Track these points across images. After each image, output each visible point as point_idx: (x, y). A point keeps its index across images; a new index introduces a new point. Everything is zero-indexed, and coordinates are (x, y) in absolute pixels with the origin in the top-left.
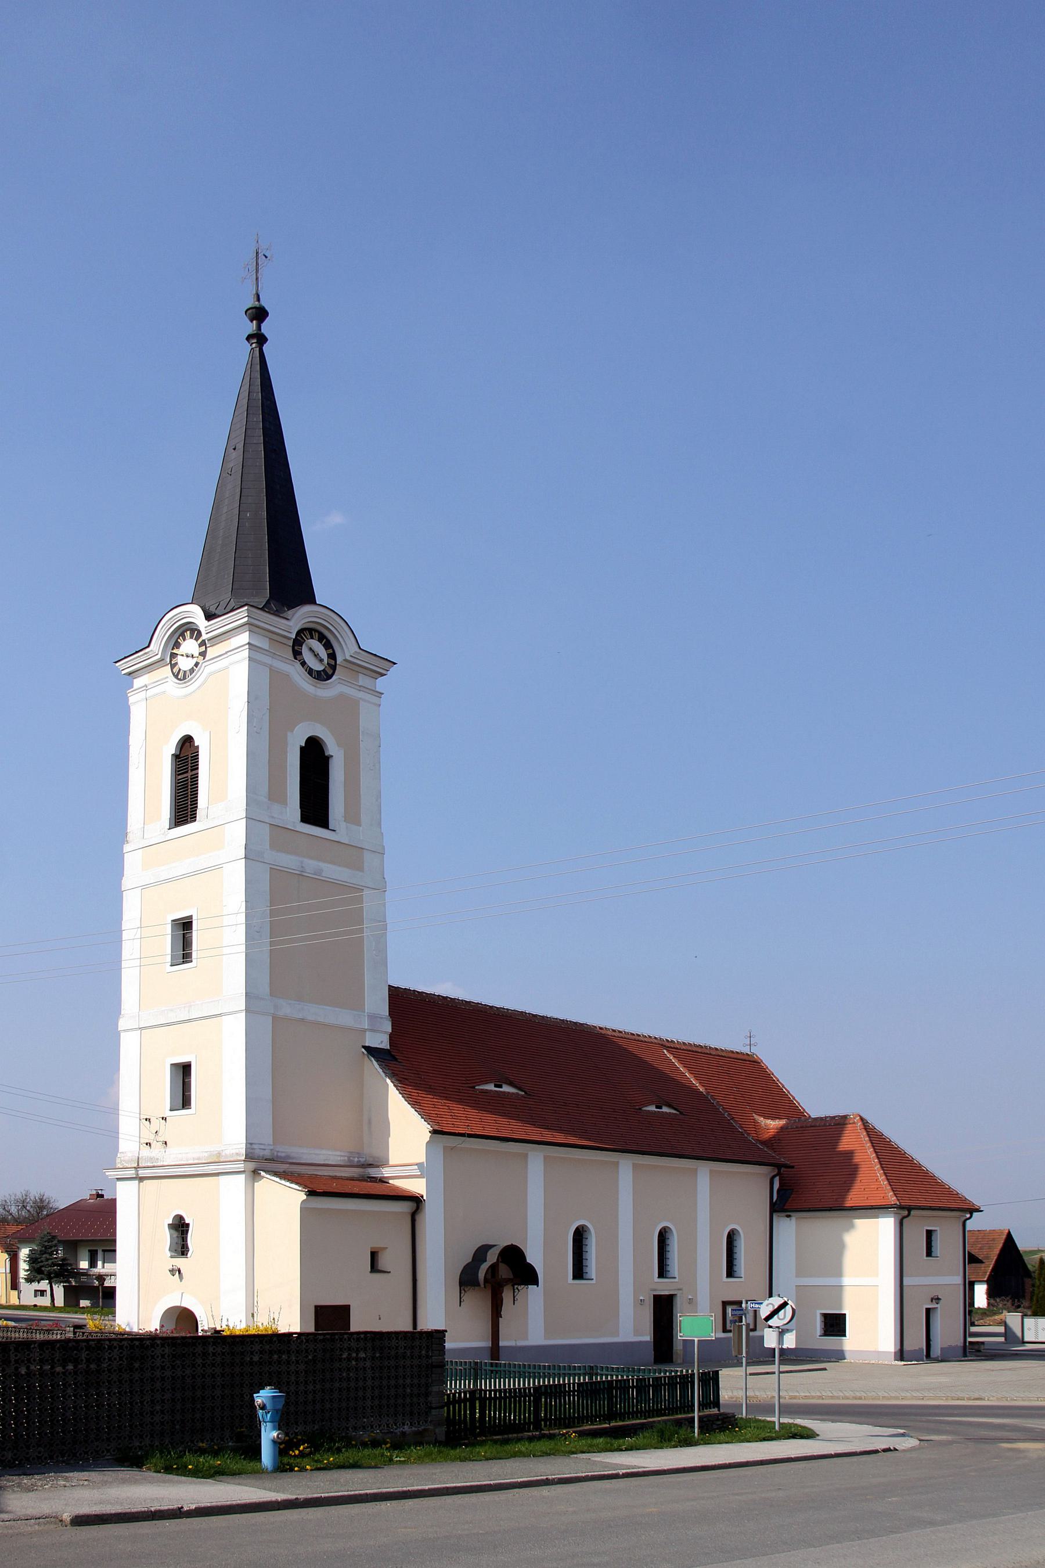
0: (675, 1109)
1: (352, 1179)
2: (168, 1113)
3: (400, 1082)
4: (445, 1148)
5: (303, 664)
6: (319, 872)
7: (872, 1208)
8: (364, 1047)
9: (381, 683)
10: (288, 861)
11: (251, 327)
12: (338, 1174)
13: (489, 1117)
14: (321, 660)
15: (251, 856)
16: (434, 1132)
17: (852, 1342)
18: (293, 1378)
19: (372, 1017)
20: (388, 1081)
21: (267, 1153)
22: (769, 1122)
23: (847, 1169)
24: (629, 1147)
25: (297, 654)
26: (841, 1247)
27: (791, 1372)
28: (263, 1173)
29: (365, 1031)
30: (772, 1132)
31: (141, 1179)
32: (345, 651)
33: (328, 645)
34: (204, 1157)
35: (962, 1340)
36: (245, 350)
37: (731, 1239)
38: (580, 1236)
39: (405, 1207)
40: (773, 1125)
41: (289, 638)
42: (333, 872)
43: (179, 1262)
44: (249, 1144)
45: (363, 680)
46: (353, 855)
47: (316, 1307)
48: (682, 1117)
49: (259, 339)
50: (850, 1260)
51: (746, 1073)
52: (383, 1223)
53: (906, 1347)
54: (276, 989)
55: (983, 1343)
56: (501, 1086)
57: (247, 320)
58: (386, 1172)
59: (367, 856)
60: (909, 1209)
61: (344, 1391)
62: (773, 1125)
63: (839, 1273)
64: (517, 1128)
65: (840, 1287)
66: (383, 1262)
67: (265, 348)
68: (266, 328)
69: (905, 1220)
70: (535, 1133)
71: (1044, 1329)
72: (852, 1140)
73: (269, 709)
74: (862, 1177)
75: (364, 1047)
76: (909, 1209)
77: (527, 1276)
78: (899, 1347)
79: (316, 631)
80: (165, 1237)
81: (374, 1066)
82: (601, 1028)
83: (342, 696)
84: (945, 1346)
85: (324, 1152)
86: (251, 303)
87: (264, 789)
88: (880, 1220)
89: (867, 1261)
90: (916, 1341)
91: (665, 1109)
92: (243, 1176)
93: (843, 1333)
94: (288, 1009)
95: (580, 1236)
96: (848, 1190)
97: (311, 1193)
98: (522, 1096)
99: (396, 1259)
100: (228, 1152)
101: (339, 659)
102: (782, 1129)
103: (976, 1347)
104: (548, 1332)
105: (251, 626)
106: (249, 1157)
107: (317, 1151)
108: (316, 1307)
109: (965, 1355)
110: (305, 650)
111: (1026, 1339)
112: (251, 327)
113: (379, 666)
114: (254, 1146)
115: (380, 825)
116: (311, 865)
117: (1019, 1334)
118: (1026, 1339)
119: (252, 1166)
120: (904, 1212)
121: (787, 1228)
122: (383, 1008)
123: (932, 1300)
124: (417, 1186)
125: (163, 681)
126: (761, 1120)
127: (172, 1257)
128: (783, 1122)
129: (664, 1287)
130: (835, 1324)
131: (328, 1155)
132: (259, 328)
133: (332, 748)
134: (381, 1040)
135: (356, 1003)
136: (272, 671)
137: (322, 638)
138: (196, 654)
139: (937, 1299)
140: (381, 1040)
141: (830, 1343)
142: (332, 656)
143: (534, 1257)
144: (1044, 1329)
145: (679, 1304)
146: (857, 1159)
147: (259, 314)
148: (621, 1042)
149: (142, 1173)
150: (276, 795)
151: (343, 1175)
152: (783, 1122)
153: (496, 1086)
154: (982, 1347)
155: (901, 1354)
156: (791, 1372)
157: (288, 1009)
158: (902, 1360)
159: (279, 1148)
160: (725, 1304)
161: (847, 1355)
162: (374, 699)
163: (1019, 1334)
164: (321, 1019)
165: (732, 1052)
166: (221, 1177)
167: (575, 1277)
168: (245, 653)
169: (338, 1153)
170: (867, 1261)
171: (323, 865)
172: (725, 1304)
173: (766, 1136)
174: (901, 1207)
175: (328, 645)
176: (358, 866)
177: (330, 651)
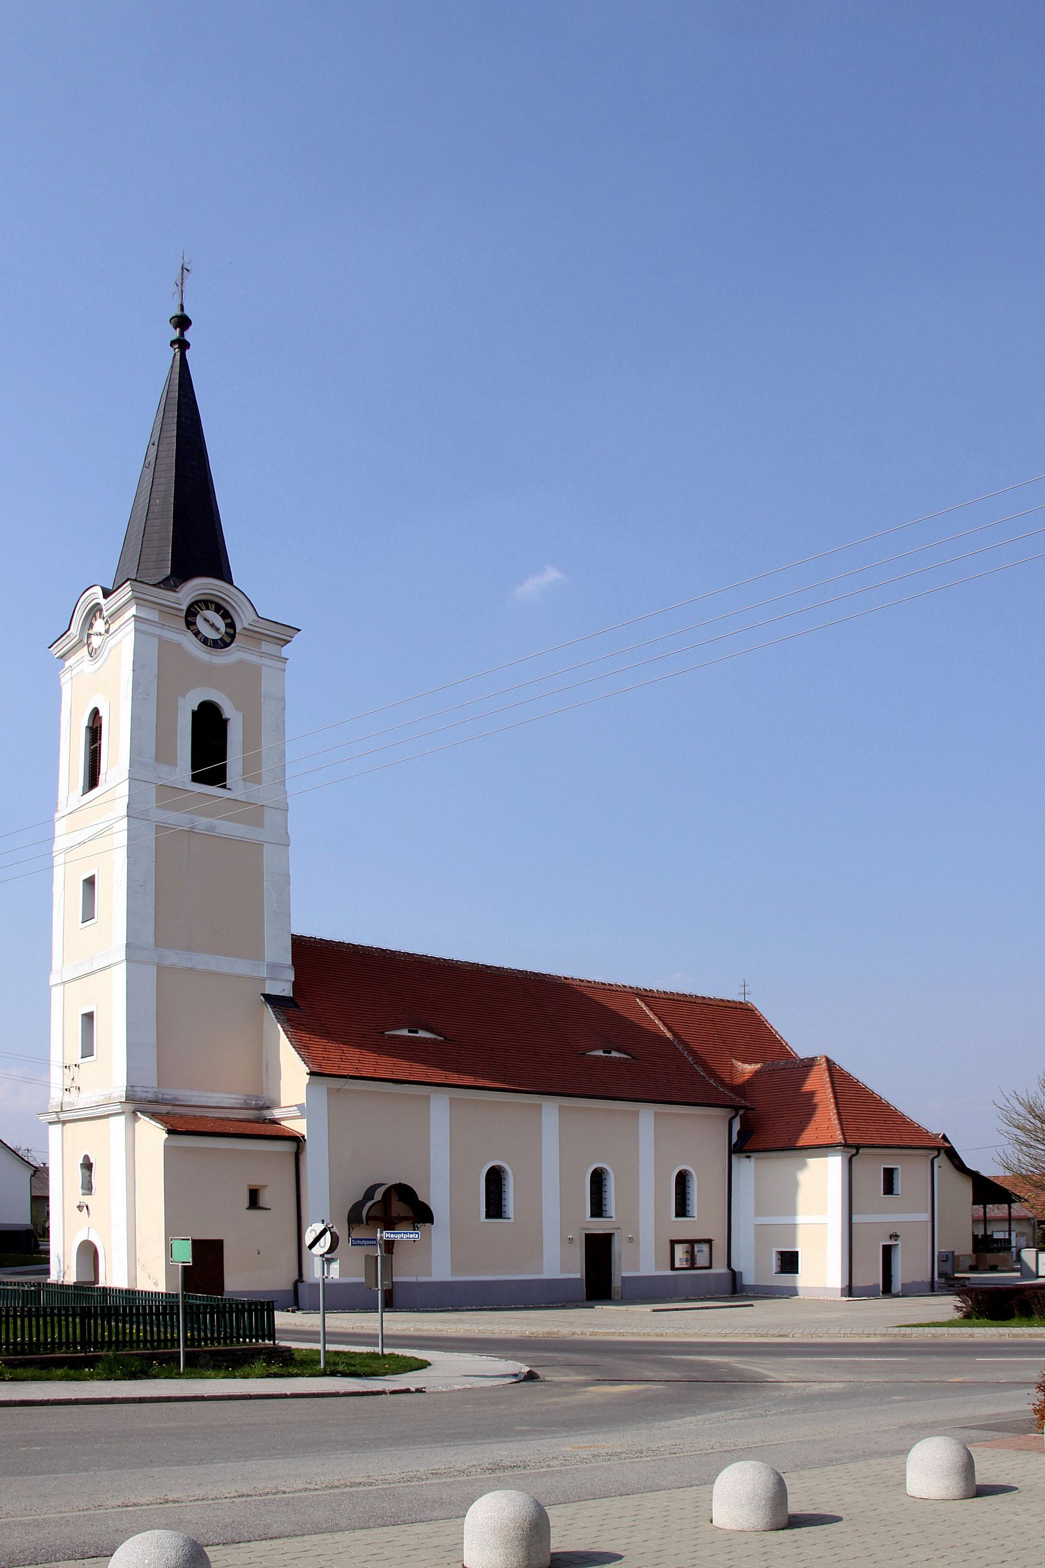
0: (626, 1054)
1: (249, 1121)
2: (80, 1061)
3: (293, 1027)
4: (329, 1090)
5: (197, 633)
6: (213, 828)
7: (820, 1147)
8: (263, 995)
9: (286, 651)
10: (179, 819)
11: (176, 334)
12: (230, 1116)
13: (389, 1061)
14: (218, 630)
15: (133, 814)
16: (311, 1074)
17: (805, 1278)
18: (56, 1311)
19: (272, 966)
20: (279, 1026)
21: (150, 1096)
22: (746, 1066)
23: (807, 1107)
24: (550, 1090)
25: (190, 624)
26: (795, 1185)
27: (707, 1308)
28: (139, 1114)
29: (264, 979)
30: (747, 1077)
31: (64, 1122)
32: (244, 620)
33: (226, 615)
34: (101, 1100)
35: (930, 1276)
36: (170, 353)
37: (682, 1179)
38: (598, 1179)
39: (289, 1147)
40: (748, 1069)
41: (181, 610)
42: (226, 828)
43: (87, 1200)
44: (130, 1087)
45: (266, 647)
46: (253, 813)
47: (222, 1241)
48: (633, 1061)
49: (182, 345)
50: (804, 1197)
51: (740, 1023)
52: (264, 1164)
53: (855, 1283)
54: (161, 940)
55: (968, 1278)
56: (416, 1032)
57: (171, 327)
58: (277, 1114)
59: (268, 813)
60: (858, 1147)
61: (207, 1324)
62: (748, 1069)
63: (793, 1211)
64: (419, 1071)
65: (794, 1226)
66: (264, 1199)
67: (188, 353)
68: (188, 335)
69: (942, 1161)
70: (438, 1075)
71: (1044, 1264)
72: (818, 1083)
73: (156, 678)
74: (819, 1117)
75: (263, 995)
76: (858, 1147)
77: (422, 1215)
78: (847, 1283)
79: (212, 602)
80: (78, 1173)
81: (269, 1011)
82: (566, 978)
83: (241, 662)
84: (909, 1281)
85: (216, 1095)
86: (177, 312)
87: (150, 749)
88: (829, 1158)
89: (817, 1196)
90: (871, 1274)
91: (614, 1054)
92: (123, 1118)
93: (795, 1271)
94: (174, 958)
95: (598, 1179)
96: (802, 1130)
97: (170, 1132)
98: (440, 1041)
99: (277, 1195)
100: (114, 1095)
101: (238, 628)
102: (757, 1073)
103: (961, 1282)
104: (455, 1269)
105: (137, 599)
106: (130, 1098)
107: (209, 1094)
108: (222, 1241)
109: (932, 1289)
110: (199, 621)
111: (1040, 1274)
112: (176, 334)
113: (282, 634)
114: (136, 1089)
115: (283, 783)
116: (202, 822)
117: (1034, 1269)
118: (1040, 1274)
119: (130, 1107)
120: (852, 1149)
121: (746, 1169)
122: (286, 957)
123: (891, 1237)
124: (299, 1127)
125: (80, 662)
126: (739, 1065)
127: (83, 1194)
128: (759, 1066)
129: (599, 1226)
130: (789, 1262)
131: (220, 1096)
132: (182, 334)
133: (228, 711)
134: (283, 988)
135: (255, 952)
136: (162, 642)
137: (219, 609)
138: (103, 632)
139: (894, 1236)
140: (283, 988)
141: (785, 1279)
142: (231, 625)
143: (437, 1196)
144: (1044, 1264)
145: (618, 1247)
146: (817, 1099)
147: (182, 322)
148: (586, 992)
149: (63, 1116)
150: (164, 755)
151: (237, 1116)
152: (759, 1066)
153: (410, 1031)
154: (967, 1282)
155: (849, 1291)
156: (707, 1308)
157: (174, 958)
158: (850, 1296)
159: (164, 1091)
160: (673, 1243)
161: (800, 1292)
162: (280, 665)
163: (1034, 1269)
164: (213, 968)
165: (723, 1001)
166: (112, 1119)
167: (677, 1215)
168: (131, 625)
169: (233, 1096)
170: (817, 1196)
171: (214, 821)
172: (673, 1243)
173: (740, 1080)
174: (846, 1145)
175: (226, 615)
176: (259, 823)
177: (229, 621)
